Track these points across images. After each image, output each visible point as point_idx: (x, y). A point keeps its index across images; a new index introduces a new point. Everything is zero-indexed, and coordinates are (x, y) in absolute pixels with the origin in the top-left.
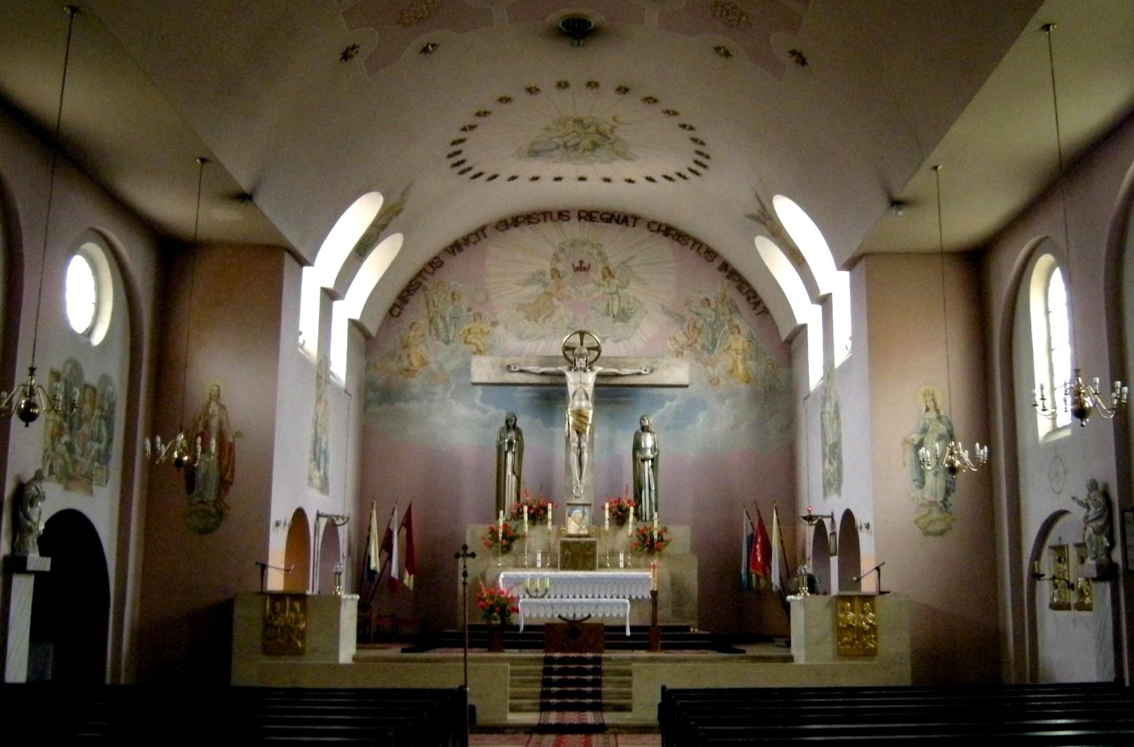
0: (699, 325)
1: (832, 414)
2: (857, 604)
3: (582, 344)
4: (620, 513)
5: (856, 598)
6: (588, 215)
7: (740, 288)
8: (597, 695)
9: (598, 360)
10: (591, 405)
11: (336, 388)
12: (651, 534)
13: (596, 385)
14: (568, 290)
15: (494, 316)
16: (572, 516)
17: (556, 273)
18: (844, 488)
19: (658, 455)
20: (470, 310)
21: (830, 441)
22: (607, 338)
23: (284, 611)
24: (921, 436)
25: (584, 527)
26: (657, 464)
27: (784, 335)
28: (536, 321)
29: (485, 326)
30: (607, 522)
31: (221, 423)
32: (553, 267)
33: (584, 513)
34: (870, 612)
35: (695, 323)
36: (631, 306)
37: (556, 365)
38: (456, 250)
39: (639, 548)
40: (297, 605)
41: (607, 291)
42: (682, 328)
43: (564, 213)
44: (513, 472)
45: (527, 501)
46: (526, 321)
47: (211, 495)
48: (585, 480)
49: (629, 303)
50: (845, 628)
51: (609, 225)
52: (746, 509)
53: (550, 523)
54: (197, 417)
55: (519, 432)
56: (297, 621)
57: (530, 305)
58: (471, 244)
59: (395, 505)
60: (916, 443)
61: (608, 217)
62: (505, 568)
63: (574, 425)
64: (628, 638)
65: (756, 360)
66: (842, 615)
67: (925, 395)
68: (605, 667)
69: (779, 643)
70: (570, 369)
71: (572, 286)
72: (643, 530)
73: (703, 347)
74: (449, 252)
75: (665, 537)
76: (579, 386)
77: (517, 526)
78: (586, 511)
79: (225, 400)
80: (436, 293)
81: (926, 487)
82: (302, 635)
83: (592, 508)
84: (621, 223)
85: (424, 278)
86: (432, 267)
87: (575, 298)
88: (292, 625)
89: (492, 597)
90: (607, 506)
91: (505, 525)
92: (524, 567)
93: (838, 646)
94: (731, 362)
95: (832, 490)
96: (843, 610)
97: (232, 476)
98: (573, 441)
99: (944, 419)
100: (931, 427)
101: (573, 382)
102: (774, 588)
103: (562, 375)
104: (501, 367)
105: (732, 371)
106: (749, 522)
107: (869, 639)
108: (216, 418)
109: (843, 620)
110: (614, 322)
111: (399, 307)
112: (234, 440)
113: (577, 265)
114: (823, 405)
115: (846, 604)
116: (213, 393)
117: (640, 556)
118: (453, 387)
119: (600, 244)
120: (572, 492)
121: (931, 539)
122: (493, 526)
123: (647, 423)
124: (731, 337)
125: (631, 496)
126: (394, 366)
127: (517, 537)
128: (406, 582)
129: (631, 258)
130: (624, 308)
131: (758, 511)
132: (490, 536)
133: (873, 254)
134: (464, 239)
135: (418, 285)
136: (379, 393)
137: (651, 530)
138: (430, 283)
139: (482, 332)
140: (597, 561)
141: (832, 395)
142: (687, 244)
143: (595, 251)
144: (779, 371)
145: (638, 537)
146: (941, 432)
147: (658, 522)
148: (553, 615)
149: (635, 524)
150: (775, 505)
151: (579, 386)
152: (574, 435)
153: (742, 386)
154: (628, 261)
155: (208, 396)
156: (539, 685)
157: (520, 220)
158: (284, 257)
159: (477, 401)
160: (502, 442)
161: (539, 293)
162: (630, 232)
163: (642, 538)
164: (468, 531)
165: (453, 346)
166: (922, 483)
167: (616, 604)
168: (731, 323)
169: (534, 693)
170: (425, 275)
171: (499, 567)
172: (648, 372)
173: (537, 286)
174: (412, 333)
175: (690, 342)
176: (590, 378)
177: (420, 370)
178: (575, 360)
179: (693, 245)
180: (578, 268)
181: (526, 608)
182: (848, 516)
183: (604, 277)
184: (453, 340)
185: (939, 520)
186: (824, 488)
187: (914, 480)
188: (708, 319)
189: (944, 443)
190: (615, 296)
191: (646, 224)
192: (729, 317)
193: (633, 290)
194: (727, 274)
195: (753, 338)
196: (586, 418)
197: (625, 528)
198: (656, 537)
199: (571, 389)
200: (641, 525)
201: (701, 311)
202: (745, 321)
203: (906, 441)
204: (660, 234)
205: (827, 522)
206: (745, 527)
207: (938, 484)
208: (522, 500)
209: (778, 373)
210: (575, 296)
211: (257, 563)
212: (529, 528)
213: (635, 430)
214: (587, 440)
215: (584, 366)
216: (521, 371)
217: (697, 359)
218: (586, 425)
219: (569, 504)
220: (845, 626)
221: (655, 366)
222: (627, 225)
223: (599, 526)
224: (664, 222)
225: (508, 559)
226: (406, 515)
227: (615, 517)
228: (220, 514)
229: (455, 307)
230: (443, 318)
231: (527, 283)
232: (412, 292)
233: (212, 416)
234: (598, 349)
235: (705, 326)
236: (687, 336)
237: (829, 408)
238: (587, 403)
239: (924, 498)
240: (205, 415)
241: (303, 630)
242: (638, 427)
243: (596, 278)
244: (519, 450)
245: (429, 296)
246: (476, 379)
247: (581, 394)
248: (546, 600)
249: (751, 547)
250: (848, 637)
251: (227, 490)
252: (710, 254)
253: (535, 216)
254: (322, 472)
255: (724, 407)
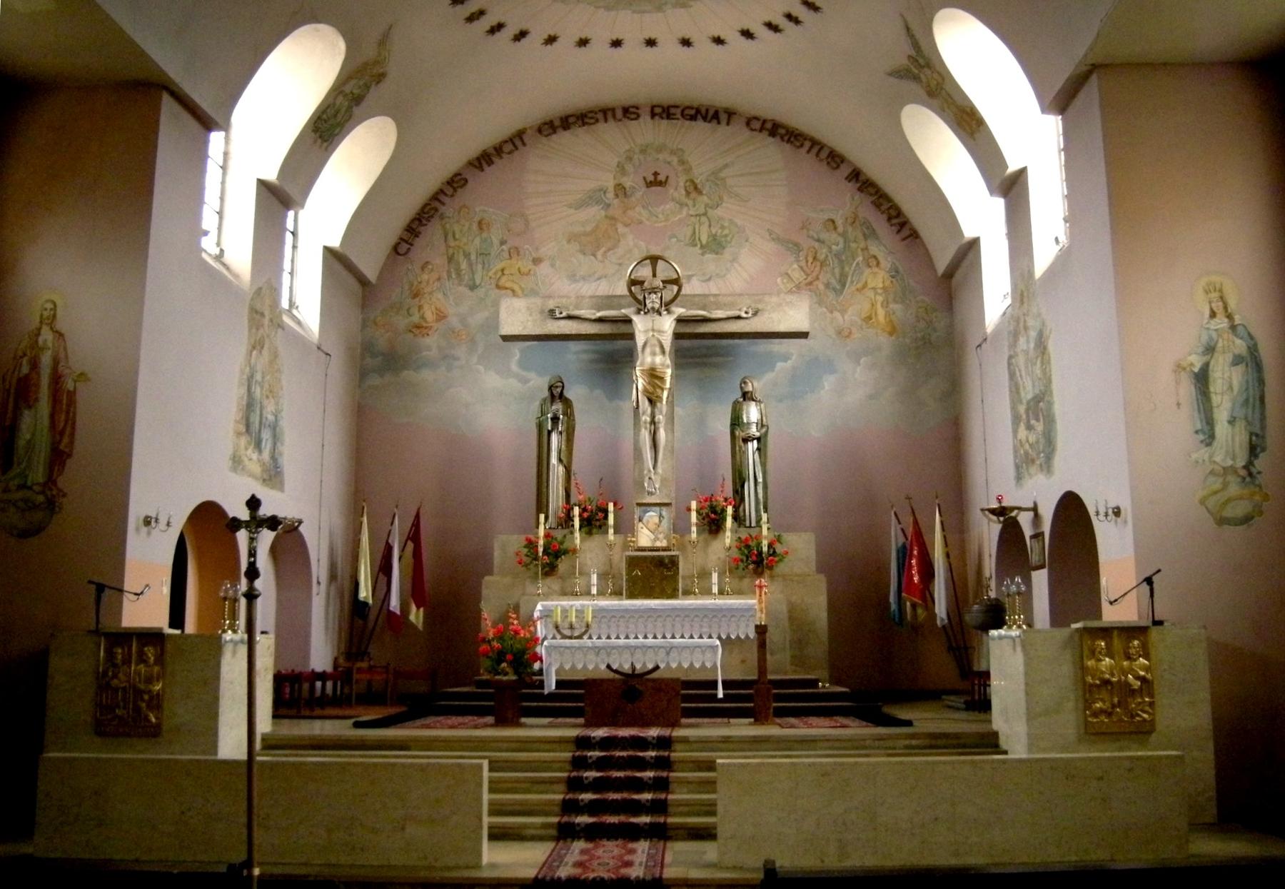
0: (821, 257)
1: (1032, 353)
2: (1117, 643)
3: (654, 275)
4: (713, 516)
5: (1115, 633)
6: (664, 112)
7: (877, 205)
8: (660, 807)
9: (679, 298)
10: (668, 362)
11: (298, 340)
12: (759, 545)
13: (677, 336)
14: (639, 212)
15: (537, 249)
16: (644, 520)
17: (621, 190)
18: (1058, 461)
19: (766, 433)
20: (503, 243)
21: (1028, 393)
22: (693, 276)
23: (127, 661)
24: (1205, 359)
25: (661, 536)
26: (765, 446)
27: (942, 263)
28: (594, 255)
29: (525, 264)
30: (694, 529)
31: (56, 362)
32: (617, 182)
33: (661, 516)
34: (1140, 656)
35: (816, 253)
36: (726, 232)
37: (620, 307)
38: (483, 162)
39: (741, 565)
40: (150, 652)
41: (691, 212)
42: (798, 261)
43: (631, 110)
44: (560, 460)
45: (579, 501)
46: (581, 257)
47: (38, 475)
48: (663, 470)
49: (723, 227)
50: (1098, 686)
51: (693, 123)
52: (895, 509)
53: (611, 531)
54: (20, 353)
55: (567, 403)
56: (149, 680)
57: (586, 234)
58: (504, 155)
59: (395, 510)
60: (1196, 370)
61: (693, 112)
62: (546, 596)
63: (645, 391)
64: (721, 701)
65: (903, 302)
66: (1091, 663)
67: (1207, 292)
68: (677, 755)
69: (950, 703)
70: (638, 312)
71: (643, 207)
72: (746, 539)
73: (827, 285)
74: (476, 167)
75: (779, 549)
76: (651, 334)
77: (565, 536)
78: (664, 513)
79: (61, 325)
80: (458, 222)
81: (1215, 444)
82: (156, 702)
83: (673, 509)
84: (710, 122)
85: (443, 204)
86: (452, 186)
87: (647, 223)
88: (142, 687)
89: (500, 636)
90: (694, 505)
91: (547, 536)
92: (575, 595)
93: (1086, 717)
94: (867, 306)
95: (1033, 470)
96: (1093, 653)
97: (72, 442)
98: (644, 414)
99: (1240, 329)
100: (1220, 344)
101: (642, 330)
102: (938, 622)
103: (628, 321)
104: (542, 312)
105: (870, 318)
106: (899, 527)
107: (1140, 703)
108: (49, 352)
109: (1095, 672)
110: (703, 254)
111: (406, 242)
112: (75, 388)
113: (651, 178)
114: (1014, 344)
115: (1097, 642)
116: (46, 314)
117: (741, 578)
118: (480, 350)
119: (681, 150)
120: (644, 488)
121: (1228, 529)
122: (532, 537)
123: (749, 388)
124: (867, 271)
125: (729, 491)
126: (401, 322)
127: (566, 552)
128: (412, 618)
129: (726, 166)
130: (716, 235)
131: (912, 509)
132: (526, 550)
133: (1106, 66)
134: (495, 149)
135: (433, 212)
136: (380, 358)
137: (758, 538)
138: (449, 209)
139: (520, 272)
140: (680, 585)
141: (1031, 323)
142: (802, 145)
143: (675, 160)
144: (936, 317)
145: (740, 549)
146: (1237, 352)
147: (768, 529)
148: (703, 663)
149: (734, 531)
150: (937, 501)
151: (651, 334)
152: (645, 404)
153: (884, 340)
154: (721, 170)
155: (38, 320)
156: (562, 787)
157: (571, 120)
158: (160, 99)
159: (514, 367)
160: (544, 417)
161: (598, 218)
162: (723, 130)
163: (746, 552)
164: (497, 546)
165: (480, 292)
166: (1209, 437)
167: (699, 647)
168: (866, 252)
169: (551, 802)
170: (442, 198)
171: (539, 594)
172: (750, 315)
173: (596, 208)
174: (425, 277)
175: (810, 279)
176: (667, 324)
177: (435, 326)
178: (645, 298)
179: (811, 148)
180: (651, 182)
181: (555, 655)
182: (1071, 507)
183: (688, 193)
184: (480, 284)
185: (1241, 498)
186: (1017, 467)
187: (1197, 432)
188: (834, 247)
189: (1244, 368)
190: (704, 219)
191: (744, 120)
192: (862, 245)
193: (727, 210)
194: (858, 185)
195: (897, 272)
196: (662, 379)
197: (720, 535)
198: (765, 549)
199: (640, 339)
200: (744, 534)
201: (824, 236)
202: (885, 248)
203: (1179, 368)
204: (765, 133)
205: (1025, 520)
206: (893, 534)
207: (1237, 439)
208: (573, 500)
209: (935, 320)
210: (648, 220)
211: (90, 582)
212: (581, 541)
213: (733, 399)
214: (664, 413)
215: (657, 306)
216: (570, 317)
217: (820, 303)
218: (663, 389)
219: (639, 505)
220: (1098, 682)
221: (760, 306)
222: (719, 123)
223: (682, 536)
224: (769, 117)
225: (553, 583)
226: (413, 525)
227: (706, 520)
228: (52, 506)
229: (484, 241)
230: (467, 255)
231: (580, 205)
232: (424, 222)
233: (42, 349)
234: (676, 282)
235: (830, 258)
236: (804, 271)
237: (1026, 344)
238: (663, 359)
239: (1215, 462)
240: (32, 348)
241: (158, 694)
242: (738, 395)
243: (676, 195)
244: (568, 429)
245: (448, 226)
246: (507, 330)
247: (654, 345)
248: (585, 641)
249: (904, 565)
250: (1102, 700)
251: (63, 464)
252: (835, 159)
253: (590, 115)
254: (266, 455)
255: (858, 369)
